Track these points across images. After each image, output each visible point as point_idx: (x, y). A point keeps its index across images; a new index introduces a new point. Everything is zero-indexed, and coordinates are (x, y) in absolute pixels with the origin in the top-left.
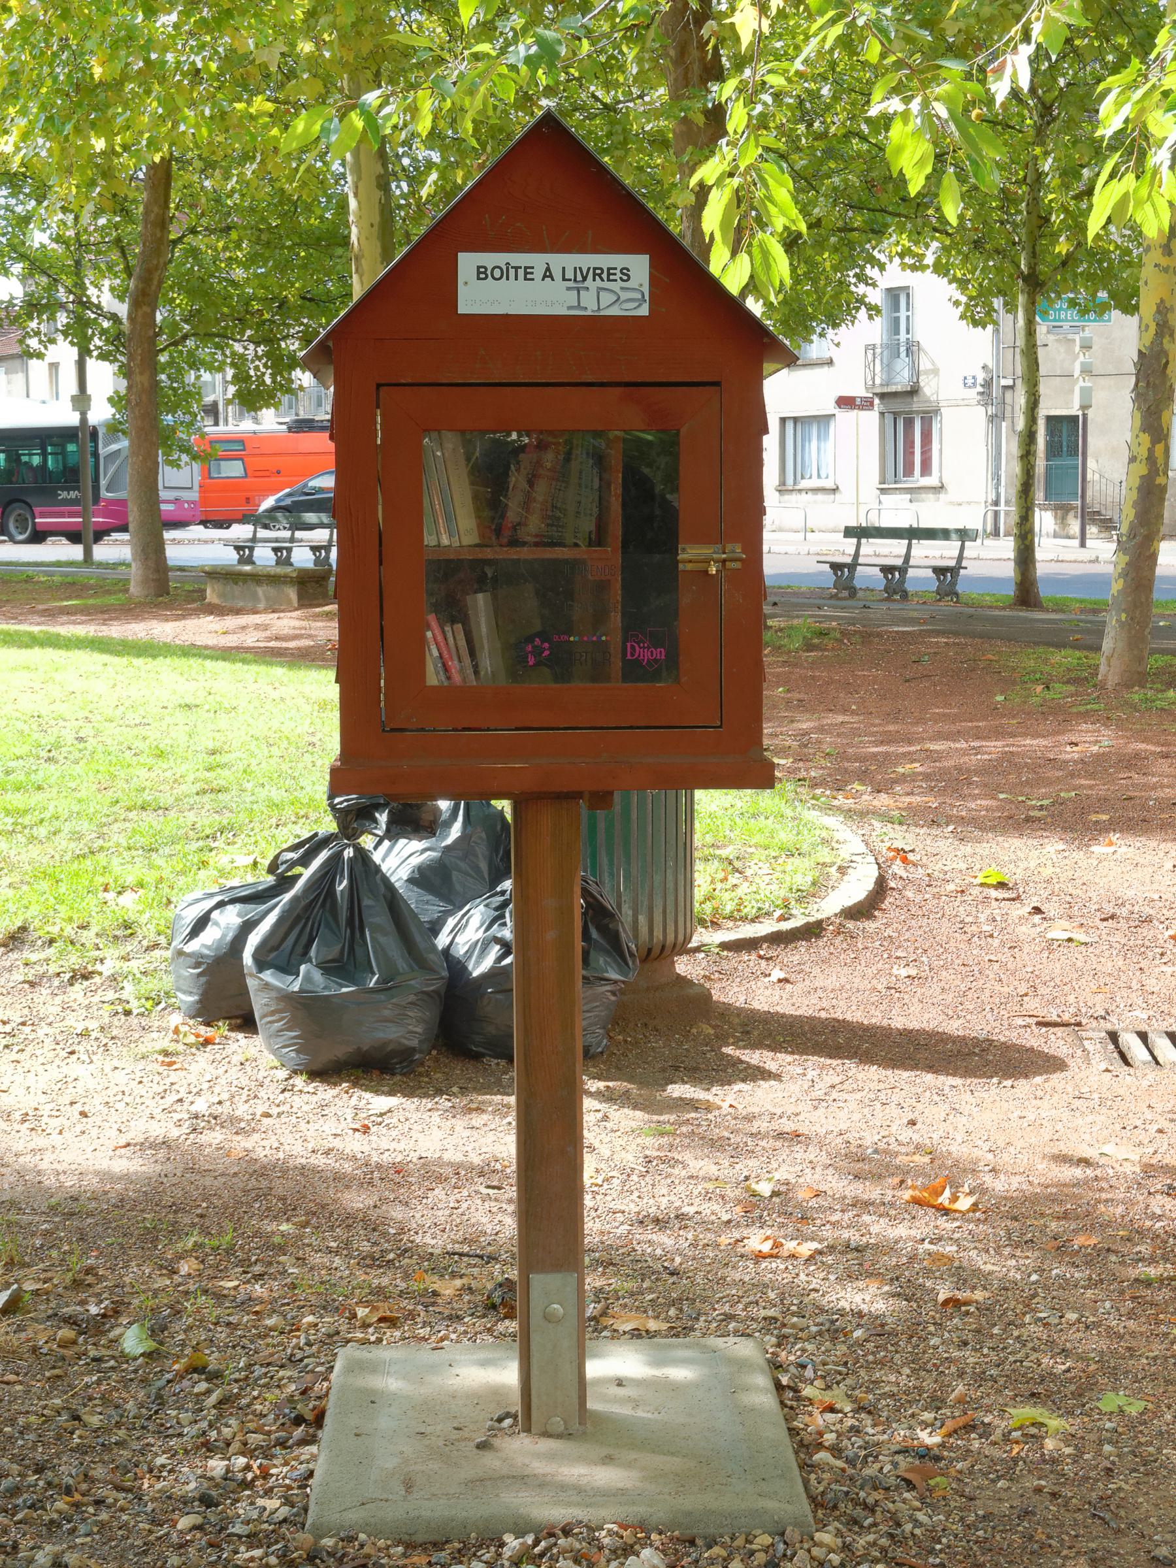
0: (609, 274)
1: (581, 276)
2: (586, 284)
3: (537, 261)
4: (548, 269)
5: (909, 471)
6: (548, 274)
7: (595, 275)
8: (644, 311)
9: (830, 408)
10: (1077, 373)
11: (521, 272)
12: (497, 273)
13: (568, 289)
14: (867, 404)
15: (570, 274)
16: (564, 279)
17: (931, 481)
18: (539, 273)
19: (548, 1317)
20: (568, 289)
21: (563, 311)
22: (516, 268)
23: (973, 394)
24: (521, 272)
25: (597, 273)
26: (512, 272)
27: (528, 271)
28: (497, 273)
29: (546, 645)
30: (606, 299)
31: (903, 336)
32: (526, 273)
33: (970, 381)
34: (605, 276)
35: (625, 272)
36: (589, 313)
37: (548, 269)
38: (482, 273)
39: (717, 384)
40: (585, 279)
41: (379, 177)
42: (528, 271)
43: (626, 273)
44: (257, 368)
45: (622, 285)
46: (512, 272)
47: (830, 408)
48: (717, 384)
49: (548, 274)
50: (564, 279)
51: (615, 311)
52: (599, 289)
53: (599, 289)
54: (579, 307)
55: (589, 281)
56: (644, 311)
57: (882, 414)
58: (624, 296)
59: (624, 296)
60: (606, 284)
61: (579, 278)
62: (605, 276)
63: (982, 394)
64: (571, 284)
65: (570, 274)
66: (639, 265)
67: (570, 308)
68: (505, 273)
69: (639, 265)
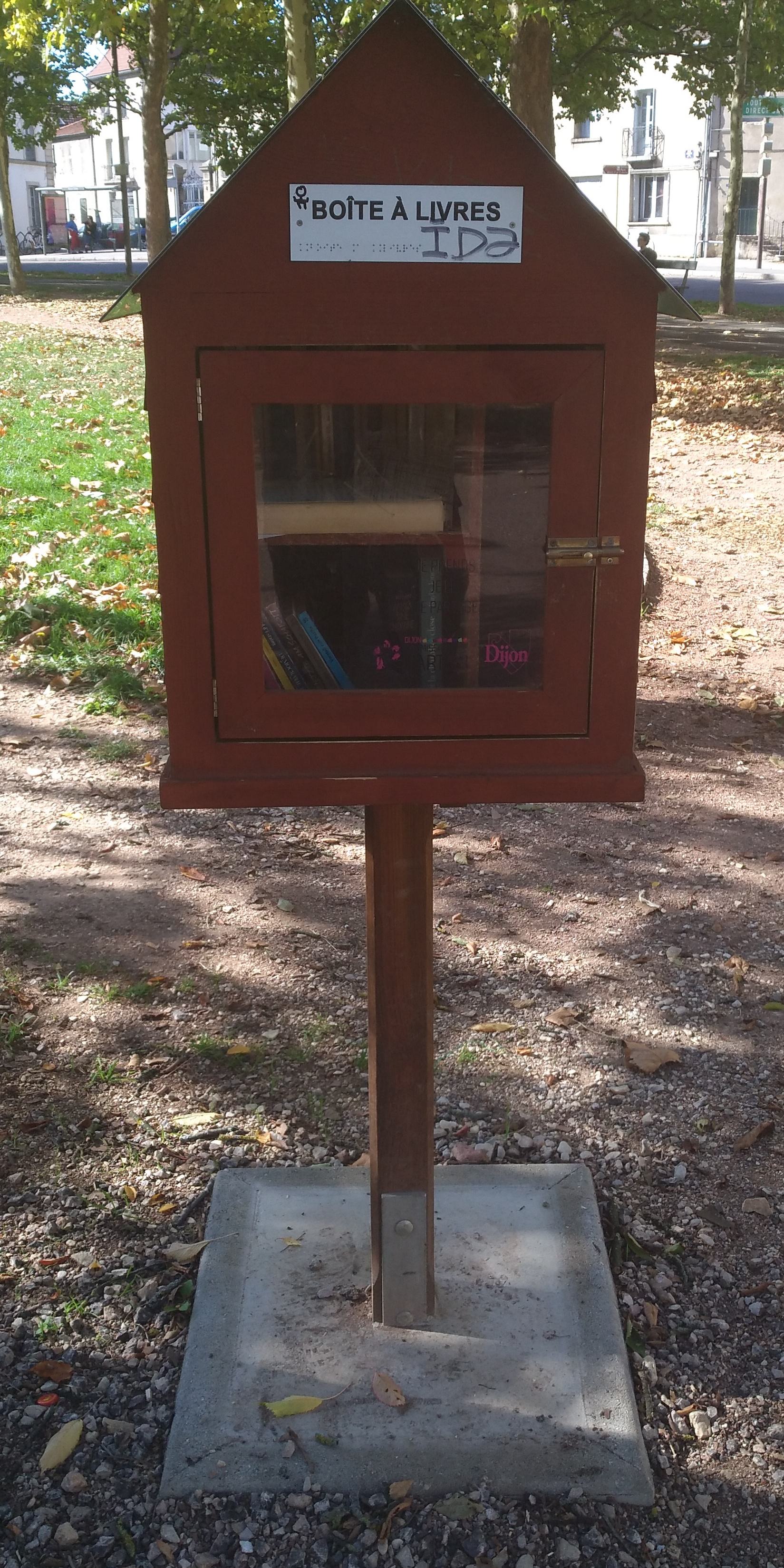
0: (474, 211)
1: (439, 215)
2: (446, 224)
3: (387, 194)
4: (400, 205)
5: (647, 214)
6: (399, 211)
7: (456, 212)
8: (516, 257)
9: (599, 172)
10: (762, 149)
11: (367, 209)
12: (338, 210)
13: (424, 230)
14: (623, 170)
15: (426, 212)
16: (419, 218)
17: (662, 220)
18: (388, 209)
19: (401, 1232)
20: (424, 230)
21: (417, 257)
22: (361, 204)
23: (691, 163)
24: (367, 209)
25: (460, 209)
26: (356, 208)
27: (375, 207)
28: (338, 210)
29: (396, 648)
30: (471, 242)
31: (648, 123)
32: (373, 210)
33: (689, 154)
34: (468, 214)
35: (494, 207)
36: (449, 260)
37: (400, 205)
38: (320, 210)
39: (600, 347)
40: (444, 217)
41: (305, 15)
42: (375, 207)
43: (494, 209)
44: (232, 146)
45: (489, 227)
46: (356, 208)
47: (599, 172)
48: (600, 347)
49: (399, 211)
50: (419, 218)
51: (480, 258)
52: (462, 230)
53: (462, 230)
54: (437, 252)
55: (449, 222)
56: (516, 257)
57: (632, 175)
58: (492, 238)
59: (492, 238)
60: (470, 224)
61: (438, 216)
62: (468, 214)
63: (697, 162)
64: (428, 224)
65: (426, 212)
66: (510, 200)
67: (425, 254)
68: (347, 209)
69: (510, 200)
